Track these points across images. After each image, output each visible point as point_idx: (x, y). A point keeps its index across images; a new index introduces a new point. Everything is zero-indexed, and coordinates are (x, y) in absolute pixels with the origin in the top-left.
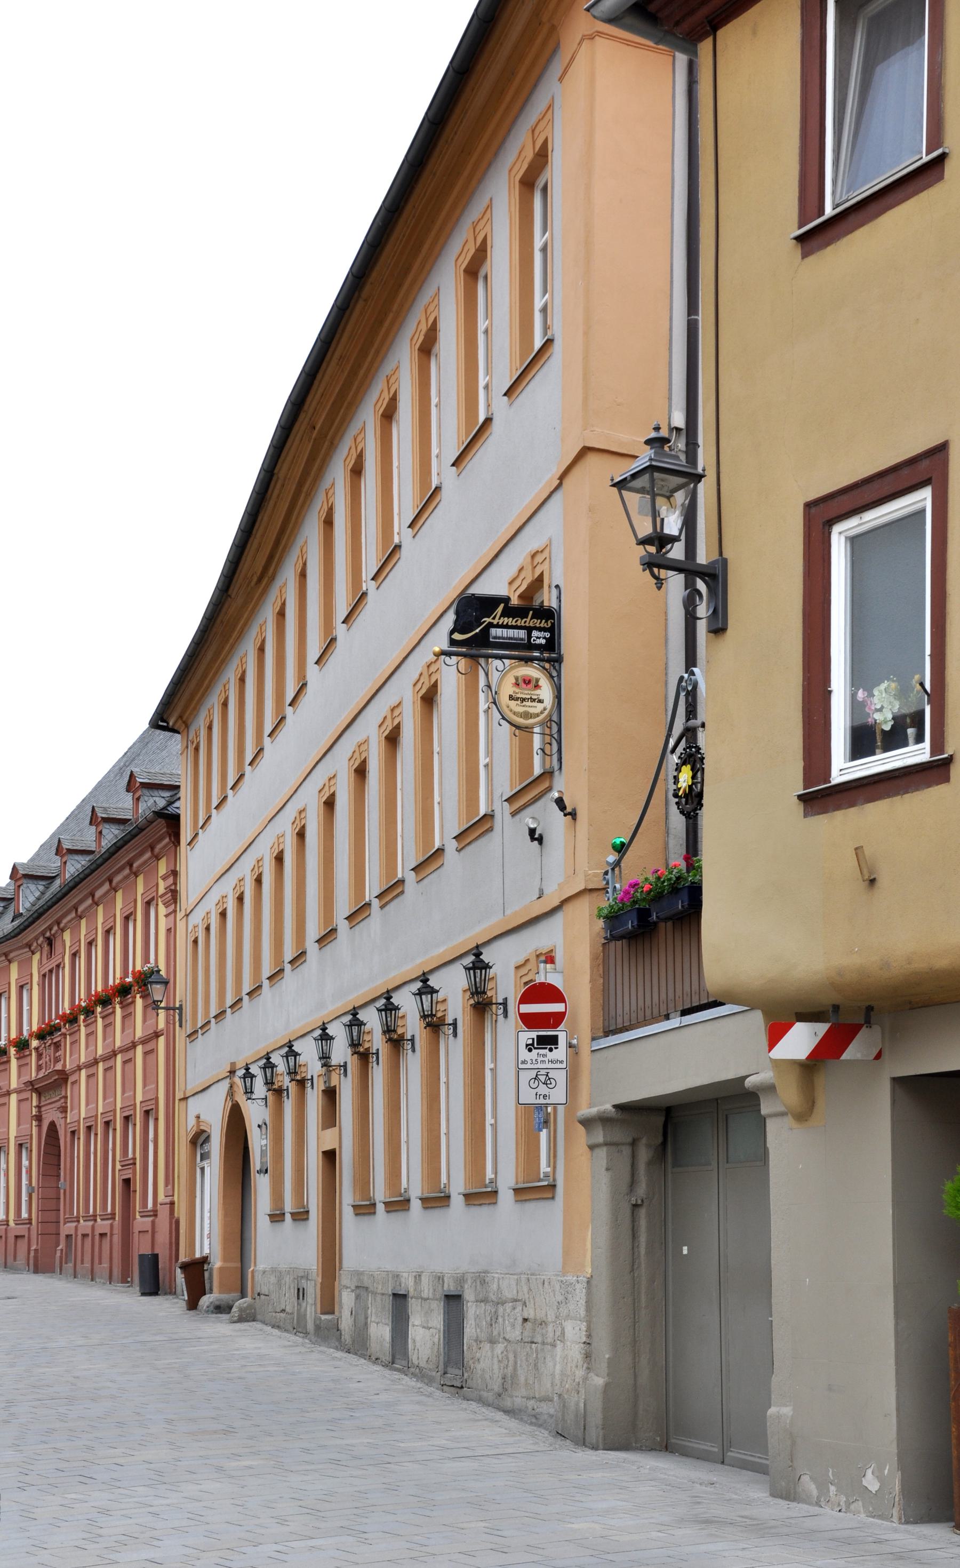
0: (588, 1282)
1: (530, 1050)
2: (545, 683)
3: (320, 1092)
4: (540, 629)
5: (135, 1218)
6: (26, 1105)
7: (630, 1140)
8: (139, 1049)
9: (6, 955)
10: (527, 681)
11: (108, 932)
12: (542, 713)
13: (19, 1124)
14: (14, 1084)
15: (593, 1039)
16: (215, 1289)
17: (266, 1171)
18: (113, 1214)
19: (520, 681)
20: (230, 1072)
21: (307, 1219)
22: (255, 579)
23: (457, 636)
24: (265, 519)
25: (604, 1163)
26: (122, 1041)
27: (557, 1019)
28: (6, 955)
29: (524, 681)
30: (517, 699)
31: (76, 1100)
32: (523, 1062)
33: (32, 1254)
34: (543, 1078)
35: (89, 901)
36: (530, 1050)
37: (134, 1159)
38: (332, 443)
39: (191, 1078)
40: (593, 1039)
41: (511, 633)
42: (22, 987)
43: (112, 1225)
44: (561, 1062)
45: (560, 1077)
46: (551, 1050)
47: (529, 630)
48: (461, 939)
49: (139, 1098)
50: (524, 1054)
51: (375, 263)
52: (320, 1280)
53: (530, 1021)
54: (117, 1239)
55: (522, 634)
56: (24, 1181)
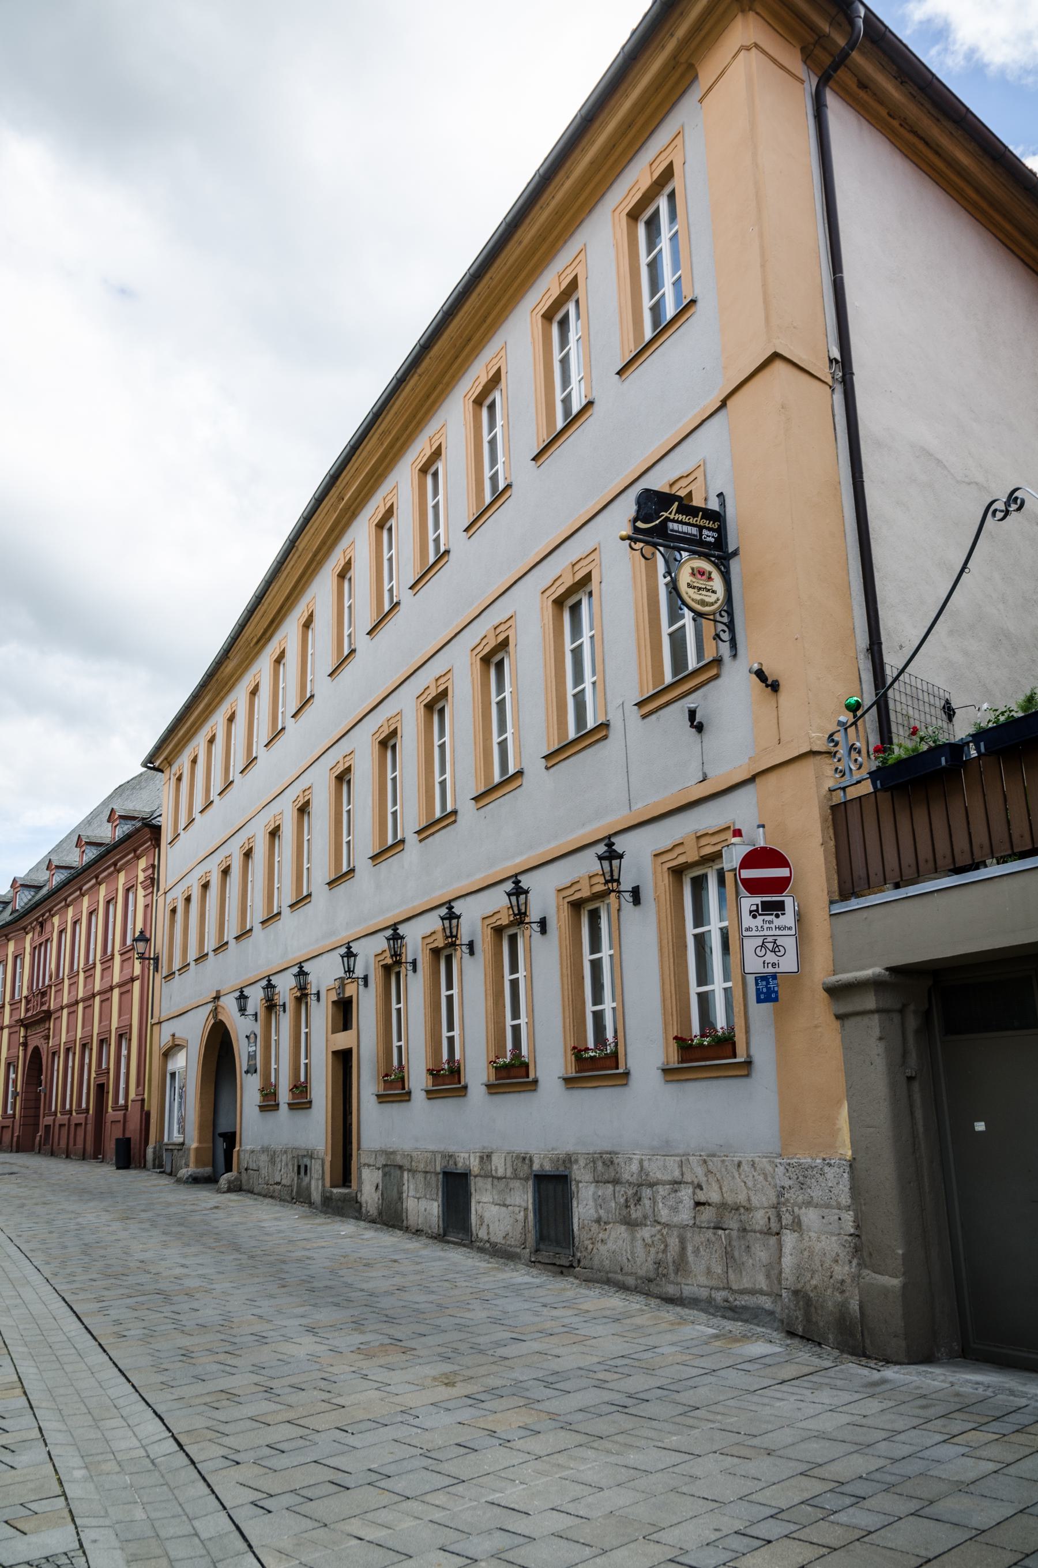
0: (851, 1166)
1: (754, 917)
2: (716, 575)
3: (330, 1004)
4: (709, 529)
5: (107, 1112)
6: (15, 1036)
7: (899, 1006)
8: (81, 1005)
9: (6, 936)
10: (702, 573)
11: (61, 932)
12: (716, 602)
13: (9, 1049)
14: (6, 1022)
15: (832, 902)
16: (192, 1164)
17: (256, 1071)
18: (87, 1109)
19: (696, 572)
20: (215, 998)
21: (310, 1108)
22: (255, 640)
23: (639, 524)
24: (276, 589)
25: (876, 1032)
26: (120, 977)
27: (780, 885)
28: (6, 936)
29: (699, 572)
30: (694, 587)
31: (57, 1031)
32: (747, 929)
33: (15, 1139)
34: (770, 946)
35: (78, 893)
36: (754, 917)
37: (108, 1069)
38: (353, 513)
39: (165, 1007)
40: (832, 902)
41: (685, 529)
42: (16, 957)
43: (86, 1118)
44: (790, 928)
45: (789, 943)
46: (777, 916)
47: (701, 528)
48: (570, 838)
49: (63, 1040)
50: (747, 921)
51: (438, 339)
52: (329, 1158)
53: (754, 887)
54: (90, 1127)
55: (694, 531)
56: (11, 1089)
